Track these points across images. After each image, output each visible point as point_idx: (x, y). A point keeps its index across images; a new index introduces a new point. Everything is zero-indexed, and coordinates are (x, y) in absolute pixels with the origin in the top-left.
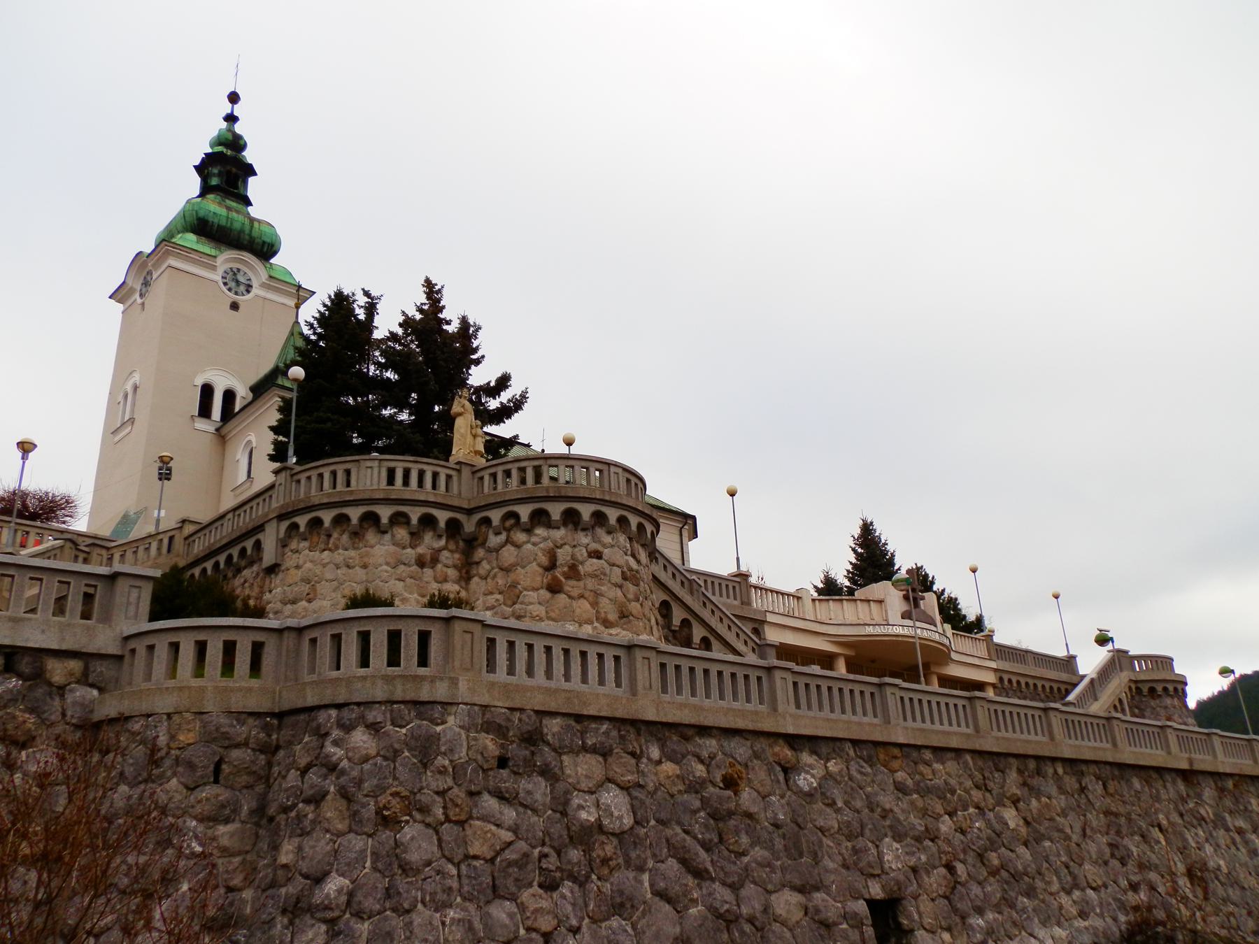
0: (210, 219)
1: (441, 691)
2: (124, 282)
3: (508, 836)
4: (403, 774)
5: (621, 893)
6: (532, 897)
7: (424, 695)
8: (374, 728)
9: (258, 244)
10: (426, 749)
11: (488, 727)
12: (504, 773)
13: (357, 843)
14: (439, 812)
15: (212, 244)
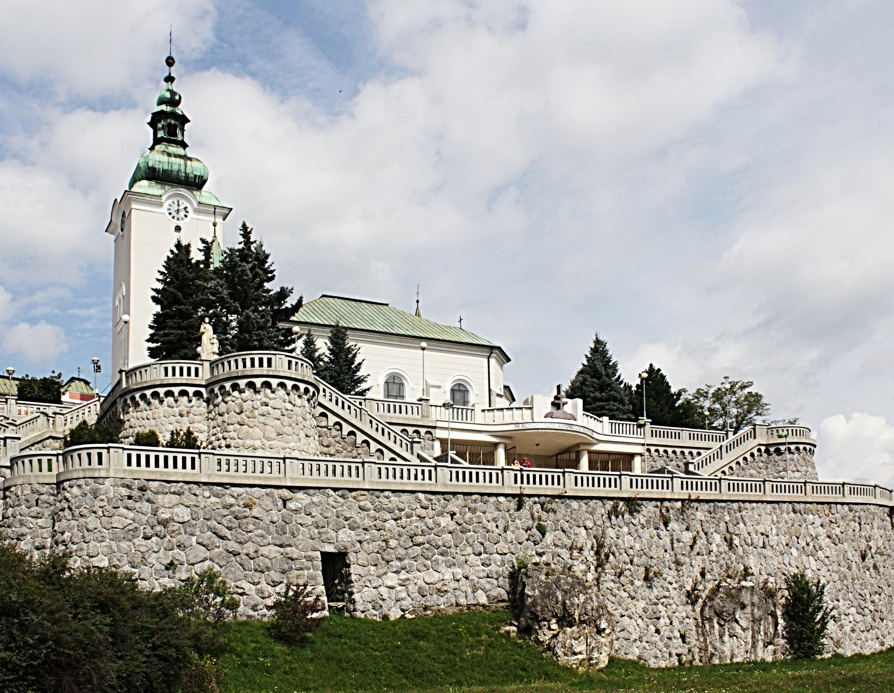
0: (157, 167)
1: (103, 474)
2: (111, 221)
3: (131, 522)
4: (88, 501)
5: (179, 542)
6: (139, 541)
7: (96, 475)
8: (79, 486)
9: (191, 178)
10: (95, 494)
11: (124, 486)
12: (130, 501)
13: (73, 522)
14: (101, 514)
15: (159, 186)
